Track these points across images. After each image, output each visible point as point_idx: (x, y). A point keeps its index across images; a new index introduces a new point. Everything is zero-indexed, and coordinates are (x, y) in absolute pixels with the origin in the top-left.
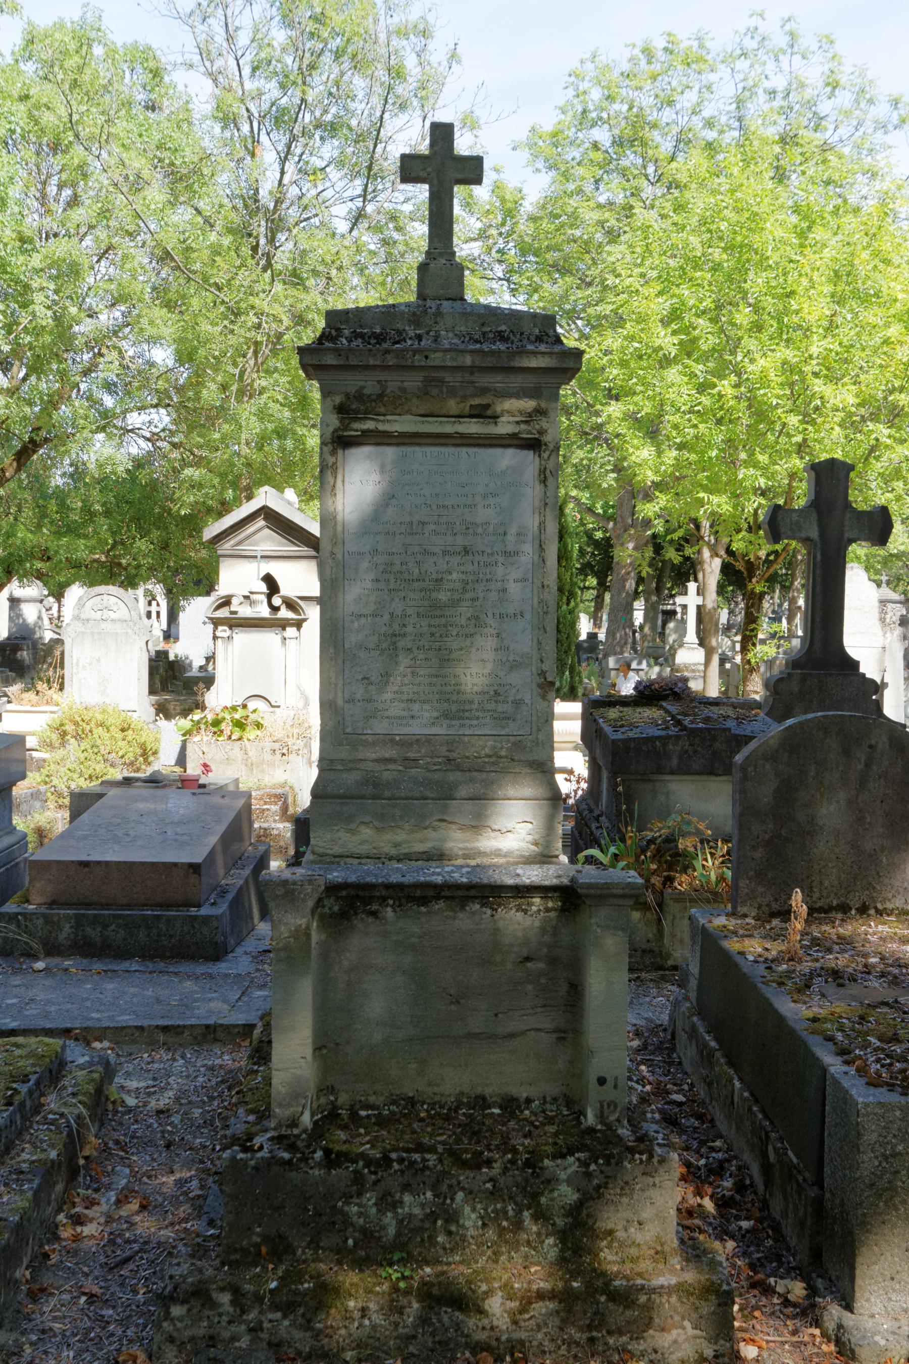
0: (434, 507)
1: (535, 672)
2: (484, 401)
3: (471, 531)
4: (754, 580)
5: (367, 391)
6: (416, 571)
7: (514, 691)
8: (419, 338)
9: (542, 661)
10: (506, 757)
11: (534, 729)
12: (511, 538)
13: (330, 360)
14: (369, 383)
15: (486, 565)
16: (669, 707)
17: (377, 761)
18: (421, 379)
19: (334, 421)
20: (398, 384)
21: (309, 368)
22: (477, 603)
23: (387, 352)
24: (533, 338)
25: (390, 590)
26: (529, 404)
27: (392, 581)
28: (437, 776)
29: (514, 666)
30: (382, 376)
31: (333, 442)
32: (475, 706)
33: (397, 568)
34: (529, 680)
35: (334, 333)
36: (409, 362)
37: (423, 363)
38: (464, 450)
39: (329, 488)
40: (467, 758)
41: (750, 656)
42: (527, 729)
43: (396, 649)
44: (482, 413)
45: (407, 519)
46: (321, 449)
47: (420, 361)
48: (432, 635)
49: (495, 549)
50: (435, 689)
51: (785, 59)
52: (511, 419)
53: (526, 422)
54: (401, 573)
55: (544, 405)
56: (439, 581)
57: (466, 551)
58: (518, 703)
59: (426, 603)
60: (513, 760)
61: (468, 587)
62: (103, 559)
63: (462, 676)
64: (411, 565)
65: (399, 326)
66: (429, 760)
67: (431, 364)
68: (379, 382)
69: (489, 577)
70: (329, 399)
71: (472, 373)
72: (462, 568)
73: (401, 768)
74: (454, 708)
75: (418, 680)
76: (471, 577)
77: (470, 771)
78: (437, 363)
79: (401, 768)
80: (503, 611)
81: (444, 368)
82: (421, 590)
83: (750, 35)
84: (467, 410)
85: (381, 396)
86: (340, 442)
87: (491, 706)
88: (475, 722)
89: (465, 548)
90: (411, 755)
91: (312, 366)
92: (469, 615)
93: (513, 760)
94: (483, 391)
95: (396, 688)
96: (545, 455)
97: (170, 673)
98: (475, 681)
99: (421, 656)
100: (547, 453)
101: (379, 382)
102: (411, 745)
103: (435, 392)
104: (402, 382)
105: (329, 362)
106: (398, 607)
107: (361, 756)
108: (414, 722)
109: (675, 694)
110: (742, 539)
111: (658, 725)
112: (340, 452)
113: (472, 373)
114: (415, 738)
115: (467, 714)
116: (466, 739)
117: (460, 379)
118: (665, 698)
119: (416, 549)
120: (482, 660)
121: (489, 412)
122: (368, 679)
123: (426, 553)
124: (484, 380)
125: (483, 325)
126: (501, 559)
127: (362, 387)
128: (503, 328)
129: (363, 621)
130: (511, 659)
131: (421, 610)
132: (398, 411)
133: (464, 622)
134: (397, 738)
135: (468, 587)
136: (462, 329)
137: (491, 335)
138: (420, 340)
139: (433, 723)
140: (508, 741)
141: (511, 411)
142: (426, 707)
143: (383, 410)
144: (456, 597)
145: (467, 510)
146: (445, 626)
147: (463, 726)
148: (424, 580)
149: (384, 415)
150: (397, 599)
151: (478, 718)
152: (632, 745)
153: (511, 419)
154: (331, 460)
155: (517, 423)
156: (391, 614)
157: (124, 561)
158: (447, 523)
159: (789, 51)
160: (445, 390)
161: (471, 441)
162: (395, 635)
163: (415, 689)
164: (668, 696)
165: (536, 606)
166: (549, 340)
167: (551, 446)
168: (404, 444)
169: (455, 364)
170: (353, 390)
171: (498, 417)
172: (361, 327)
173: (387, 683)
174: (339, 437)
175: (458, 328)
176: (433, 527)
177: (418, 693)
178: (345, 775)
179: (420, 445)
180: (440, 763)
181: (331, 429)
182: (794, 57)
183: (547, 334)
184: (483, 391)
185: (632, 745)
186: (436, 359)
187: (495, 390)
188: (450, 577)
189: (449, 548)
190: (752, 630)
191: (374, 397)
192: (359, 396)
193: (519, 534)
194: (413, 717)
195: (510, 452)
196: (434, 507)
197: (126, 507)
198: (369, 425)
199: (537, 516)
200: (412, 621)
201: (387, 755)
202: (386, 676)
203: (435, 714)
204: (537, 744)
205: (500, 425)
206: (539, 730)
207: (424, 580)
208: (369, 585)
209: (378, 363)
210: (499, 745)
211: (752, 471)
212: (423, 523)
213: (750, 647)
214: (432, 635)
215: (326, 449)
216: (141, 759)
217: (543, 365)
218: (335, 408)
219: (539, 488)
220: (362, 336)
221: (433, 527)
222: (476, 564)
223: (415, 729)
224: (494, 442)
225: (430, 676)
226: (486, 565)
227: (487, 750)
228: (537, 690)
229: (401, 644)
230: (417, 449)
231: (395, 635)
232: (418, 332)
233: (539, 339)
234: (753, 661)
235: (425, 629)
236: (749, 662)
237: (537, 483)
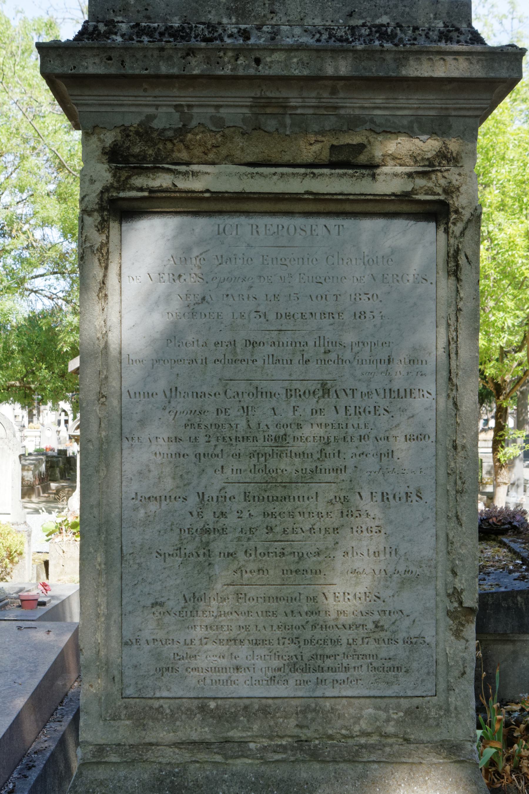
0: (272, 317)
1: (442, 592)
2: (355, 140)
3: (333, 356)
4: (501, 398)
5: (157, 124)
6: (243, 424)
7: (407, 622)
8: (245, 35)
9: (454, 573)
10: (396, 736)
11: (442, 686)
12: (399, 368)
13: (93, 66)
14: (160, 110)
15: (358, 412)
16: (512, 545)
17: (178, 745)
18: (248, 102)
19: (104, 174)
20: (212, 110)
21: (59, 82)
22: (343, 476)
23: (191, 52)
24: (434, 35)
25: (198, 456)
26: (430, 145)
27: (202, 440)
28: (280, 772)
29: (408, 580)
30: (185, 97)
31: (101, 209)
32: (341, 649)
33: (210, 418)
34: (431, 604)
35: (102, 28)
36: (228, 71)
37: (252, 72)
38: (322, 221)
39: (95, 286)
40: (331, 737)
41: (500, 455)
42: (430, 685)
43: (209, 554)
44: (350, 159)
45: (226, 337)
46: (82, 220)
47: (248, 66)
48: (270, 529)
49: (373, 386)
50: (276, 621)
51: (507, 23)
52: (400, 169)
53: (424, 174)
54: (217, 426)
55: (454, 145)
56: (280, 440)
57: (325, 390)
58: (414, 643)
59: (259, 477)
60: (407, 740)
61: (329, 450)
62: (18, 384)
63: (321, 598)
64: (233, 412)
65: (212, 18)
66: (266, 742)
67: (267, 72)
68: (177, 107)
69: (363, 432)
70: (94, 139)
71: (334, 92)
72: (320, 419)
73: (218, 758)
74: (307, 651)
75: (245, 606)
76: (335, 433)
77: (334, 761)
78: (276, 71)
79: (218, 758)
80: (388, 489)
81: (286, 80)
82: (251, 455)
83: (482, 5)
84: (325, 156)
85: (182, 131)
86: (112, 208)
87: (371, 648)
88: (342, 676)
89: (324, 385)
90: (235, 734)
91: (62, 77)
92: (331, 496)
93: (407, 740)
94: (354, 123)
95: (209, 620)
96: (457, 229)
97: (67, 466)
98: (342, 605)
99: (252, 566)
100: (460, 226)
101: (177, 107)
102: (234, 717)
103: (271, 124)
104: (218, 107)
105: (92, 70)
106: (214, 483)
107: (151, 737)
108: (241, 676)
109: (515, 528)
110: (493, 366)
111: (511, 572)
112: (114, 226)
113: (334, 92)
114: (242, 703)
115: (329, 662)
116: (328, 704)
117: (313, 102)
118: (504, 532)
119: (242, 387)
120: (354, 571)
121: (362, 159)
122: (162, 604)
123: (258, 392)
124: (356, 104)
125: (351, 15)
126: (383, 403)
127: (151, 118)
128: (385, 20)
129: (153, 507)
130: (401, 568)
131: (250, 488)
132: (211, 156)
133: (322, 507)
134: (212, 705)
135: (329, 450)
136: (318, 21)
137: (365, 31)
138: (247, 38)
139: (272, 679)
140: (398, 707)
141: (398, 158)
142: (261, 651)
143: (184, 155)
144: (309, 465)
145: (326, 322)
146: (291, 514)
147: (323, 681)
148: (255, 439)
149: (188, 164)
150: (210, 471)
151: (347, 669)
152: (490, 601)
153: (400, 169)
154: (98, 238)
155: (410, 175)
156: (201, 496)
157: (33, 386)
158: (294, 343)
159: (510, 16)
160: (288, 121)
161: (333, 207)
162: (208, 531)
163: (242, 620)
164: (507, 530)
165: (442, 479)
166: (462, 38)
167: (466, 214)
168: (221, 213)
169: (306, 72)
170: (134, 121)
171: (378, 166)
172: (148, 18)
173: (194, 612)
174: (113, 201)
175: (309, 21)
176: (269, 350)
177: (246, 628)
178: (122, 773)
179: (247, 213)
180: (284, 749)
181: (98, 187)
182: (514, 20)
183: (457, 30)
184: (354, 123)
185: (490, 601)
186: (275, 64)
187: (372, 121)
188: (298, 434)
189: (297, 385)
190: (501, 436)
191: (170, 134)
192: (145, 133)
193: (412, 361)
194: (237, 668)
195: (399, 224)
196: (272, 317)
197: (35, 347)
198: (163, 181)
199: (442, 330)
200: (236, 507)
201: (195, 736)
202: (193, 600)
203: (276, 663)
204: (448, 711)
205: (380, 178)
206: (450, 689)
207: (255, 439)
208: (162, 447)
209: (175, 71)
210: (383, 715)
211: (501, 314)
212: (253, 344)
213: (500, 449)
214: (270, 529)
215: (89, 220)
216: (7, 560)
217: (456, 74)
218: (104, 153)
219: (445, 286)
220: (150, 32)
221: (269, 350)
222: (342, 411)
223: (244, 688)
224: (369, 208)
225: (267, 599)
226: (358, 412)
227: (363, 725)
228: (445, 622)
229: (218, 545)
230: (243, 220)
231: (208, 531)
232: (243, 27)
233: (445, 36)
234: (502, 459)
235: (258, 520)
236: (499, 460)
237: (442, 274)
